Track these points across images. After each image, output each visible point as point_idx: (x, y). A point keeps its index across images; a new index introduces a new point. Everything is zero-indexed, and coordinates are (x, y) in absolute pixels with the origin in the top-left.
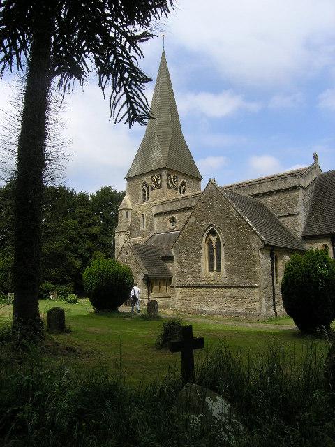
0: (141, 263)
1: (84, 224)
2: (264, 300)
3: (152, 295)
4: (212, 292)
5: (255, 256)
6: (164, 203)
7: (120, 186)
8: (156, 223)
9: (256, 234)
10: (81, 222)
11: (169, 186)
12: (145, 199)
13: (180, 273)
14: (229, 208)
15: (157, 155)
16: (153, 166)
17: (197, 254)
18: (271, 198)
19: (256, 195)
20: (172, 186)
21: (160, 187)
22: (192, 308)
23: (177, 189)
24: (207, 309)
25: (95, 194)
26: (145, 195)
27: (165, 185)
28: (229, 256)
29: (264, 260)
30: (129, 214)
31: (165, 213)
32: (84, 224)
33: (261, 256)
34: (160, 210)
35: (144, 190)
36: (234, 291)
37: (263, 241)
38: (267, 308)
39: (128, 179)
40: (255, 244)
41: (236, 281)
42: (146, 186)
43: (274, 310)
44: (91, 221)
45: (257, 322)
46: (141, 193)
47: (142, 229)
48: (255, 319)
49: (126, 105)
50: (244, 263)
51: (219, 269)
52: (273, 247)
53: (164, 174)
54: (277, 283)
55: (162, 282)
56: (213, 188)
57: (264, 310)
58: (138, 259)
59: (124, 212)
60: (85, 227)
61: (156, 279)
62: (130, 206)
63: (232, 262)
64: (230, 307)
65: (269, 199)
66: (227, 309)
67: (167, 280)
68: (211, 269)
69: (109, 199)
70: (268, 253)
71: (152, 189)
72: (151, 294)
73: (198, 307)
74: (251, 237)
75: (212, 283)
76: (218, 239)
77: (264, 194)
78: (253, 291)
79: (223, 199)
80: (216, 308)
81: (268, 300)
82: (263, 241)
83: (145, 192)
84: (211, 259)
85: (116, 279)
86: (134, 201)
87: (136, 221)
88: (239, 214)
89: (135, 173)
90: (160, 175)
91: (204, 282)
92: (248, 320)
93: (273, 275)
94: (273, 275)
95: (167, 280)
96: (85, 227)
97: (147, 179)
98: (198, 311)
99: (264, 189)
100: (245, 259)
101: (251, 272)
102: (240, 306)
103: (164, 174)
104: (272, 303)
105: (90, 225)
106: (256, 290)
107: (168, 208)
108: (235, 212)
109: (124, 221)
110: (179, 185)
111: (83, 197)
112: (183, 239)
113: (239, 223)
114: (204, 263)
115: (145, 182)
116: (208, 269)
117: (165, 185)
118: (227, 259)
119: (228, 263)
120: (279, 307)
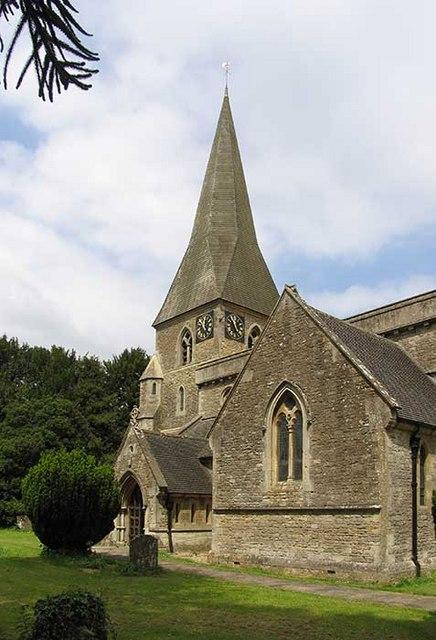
0: (156, 467)
1: (89, 408)
2: (391, 539)
3: (176, 526)
4: (361, 529)
5: (376, 444)
6: (216, 363)
7: (147, 341)
8: (201, 401)
9: (380, 395)
10: (83, 404)
11: (227, 336)
12: (185, 360)
13: (223, 485)
14: (321, 344)
15: (208, 280)
16: (200, 299)
17: (257, 445)
18: (417, 338)
19: (387, 334)
20: (232, 334)
21: (211, 336)
22: (240, 554)
23: (242, 341)
24: (269, 553)
25: (112, 360)
26: (185, 354)
27: (219, 330)
28: (320, 444)
29: (395, 454)
30: (158, 387)
31: (217, 382)
32: (89, 408)
33: (389, 442)
34: (209, 376)
35: (184, 345)
36: (328, 518)
37: (394, 409)
38: (399, 556)
39: (157, 326)
40: (377, 416)
41: (333, 499)
42: (187, 337)
43: (415, 559)
44: (100, 404)
45: (374, 586)
46: (178, 348)
47: (179, 413)
48: (367, 578)
49: (26, 25)
50: (349, 458)
51: (298, 475)
52: (418, 424)
53: (219, 312)
54: (422, 503)
55: (197, 503)
56: (291, 304)
57: (391, 559)
58: (151, 458)
59: (150, 383)
60: (91, 412)
61: (185, 497)
62: (159, 374)
63: (327, 458)
64: (319, 554)
65: (413, 340)
66: (310, 556)
67: (202, 501)
68: (283, 476)
69: (133, 364)
70: (406, 437)
71: (198, 341)
72: (174, 523)
73: (255, 551)
74: (368, 403)
75: (284, 504)
76: (299, 412)
77: (404, 331)
78: (367, 519)
79: (312, 325)
80: (290, 555)
81: (399, 540)
82: (394, 409)
83: (185, 348)
84: (283, 456)
85: (79, 491)
86: (167, 364)
87: (169, 400)
88: (344, 354)
89: (170, 315)
90: (212, 313)
91: (267, 502)
92: (355, 582)
93: (414, 485)
94: (414, 485)
95: (202, 501)
96: (91, 412)
97: (189, 323)
98: (254, 559)
99: (404, 319)
100: (353, 451)
101: (364, 479)
102: (339, 550)
103: (219, 312)
104: (409, 545)
105: (98, 411)
106: (375, 518)
107: (222, 372)
108: (335, 351)
109: (150, 398)
110: (248, 332)
111: (91, 365)
112: (229, 417)
113: (344, 373)
114: (269, 462)
115: (186, 330)
116: (275, 476)
117: (219, 330)
118: (315, 453)
119: (316, 461)
120: (425, 555)
